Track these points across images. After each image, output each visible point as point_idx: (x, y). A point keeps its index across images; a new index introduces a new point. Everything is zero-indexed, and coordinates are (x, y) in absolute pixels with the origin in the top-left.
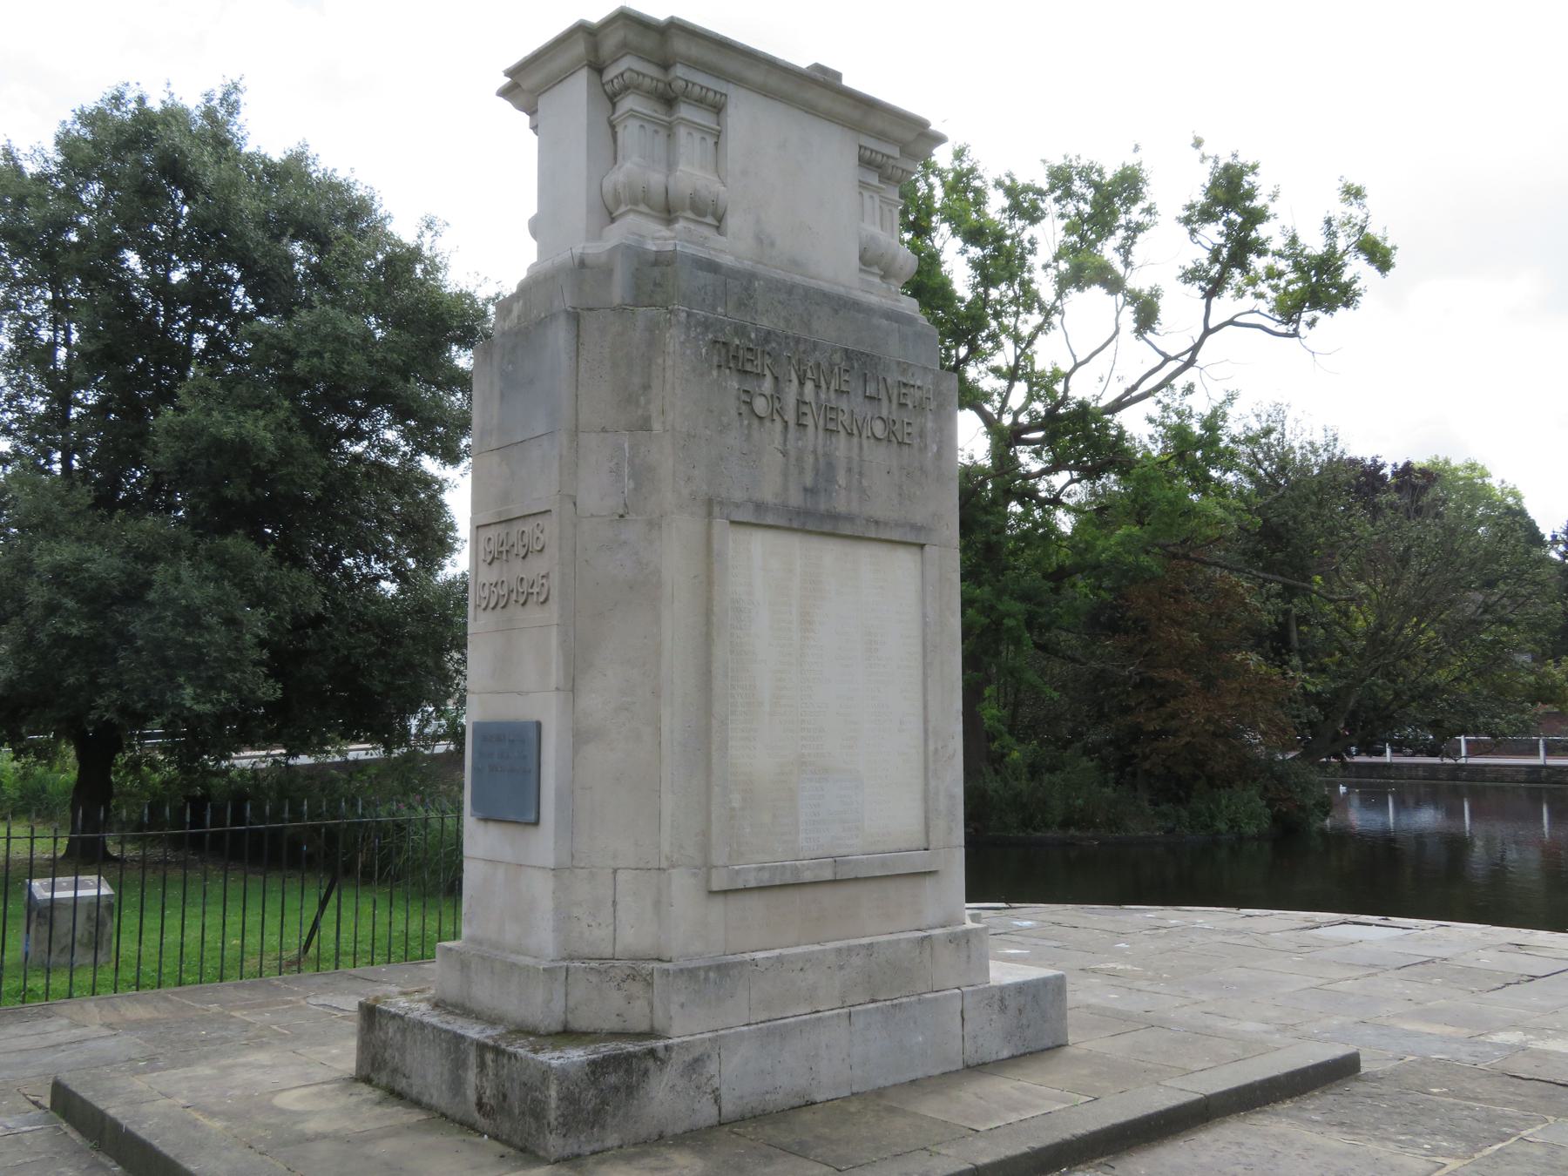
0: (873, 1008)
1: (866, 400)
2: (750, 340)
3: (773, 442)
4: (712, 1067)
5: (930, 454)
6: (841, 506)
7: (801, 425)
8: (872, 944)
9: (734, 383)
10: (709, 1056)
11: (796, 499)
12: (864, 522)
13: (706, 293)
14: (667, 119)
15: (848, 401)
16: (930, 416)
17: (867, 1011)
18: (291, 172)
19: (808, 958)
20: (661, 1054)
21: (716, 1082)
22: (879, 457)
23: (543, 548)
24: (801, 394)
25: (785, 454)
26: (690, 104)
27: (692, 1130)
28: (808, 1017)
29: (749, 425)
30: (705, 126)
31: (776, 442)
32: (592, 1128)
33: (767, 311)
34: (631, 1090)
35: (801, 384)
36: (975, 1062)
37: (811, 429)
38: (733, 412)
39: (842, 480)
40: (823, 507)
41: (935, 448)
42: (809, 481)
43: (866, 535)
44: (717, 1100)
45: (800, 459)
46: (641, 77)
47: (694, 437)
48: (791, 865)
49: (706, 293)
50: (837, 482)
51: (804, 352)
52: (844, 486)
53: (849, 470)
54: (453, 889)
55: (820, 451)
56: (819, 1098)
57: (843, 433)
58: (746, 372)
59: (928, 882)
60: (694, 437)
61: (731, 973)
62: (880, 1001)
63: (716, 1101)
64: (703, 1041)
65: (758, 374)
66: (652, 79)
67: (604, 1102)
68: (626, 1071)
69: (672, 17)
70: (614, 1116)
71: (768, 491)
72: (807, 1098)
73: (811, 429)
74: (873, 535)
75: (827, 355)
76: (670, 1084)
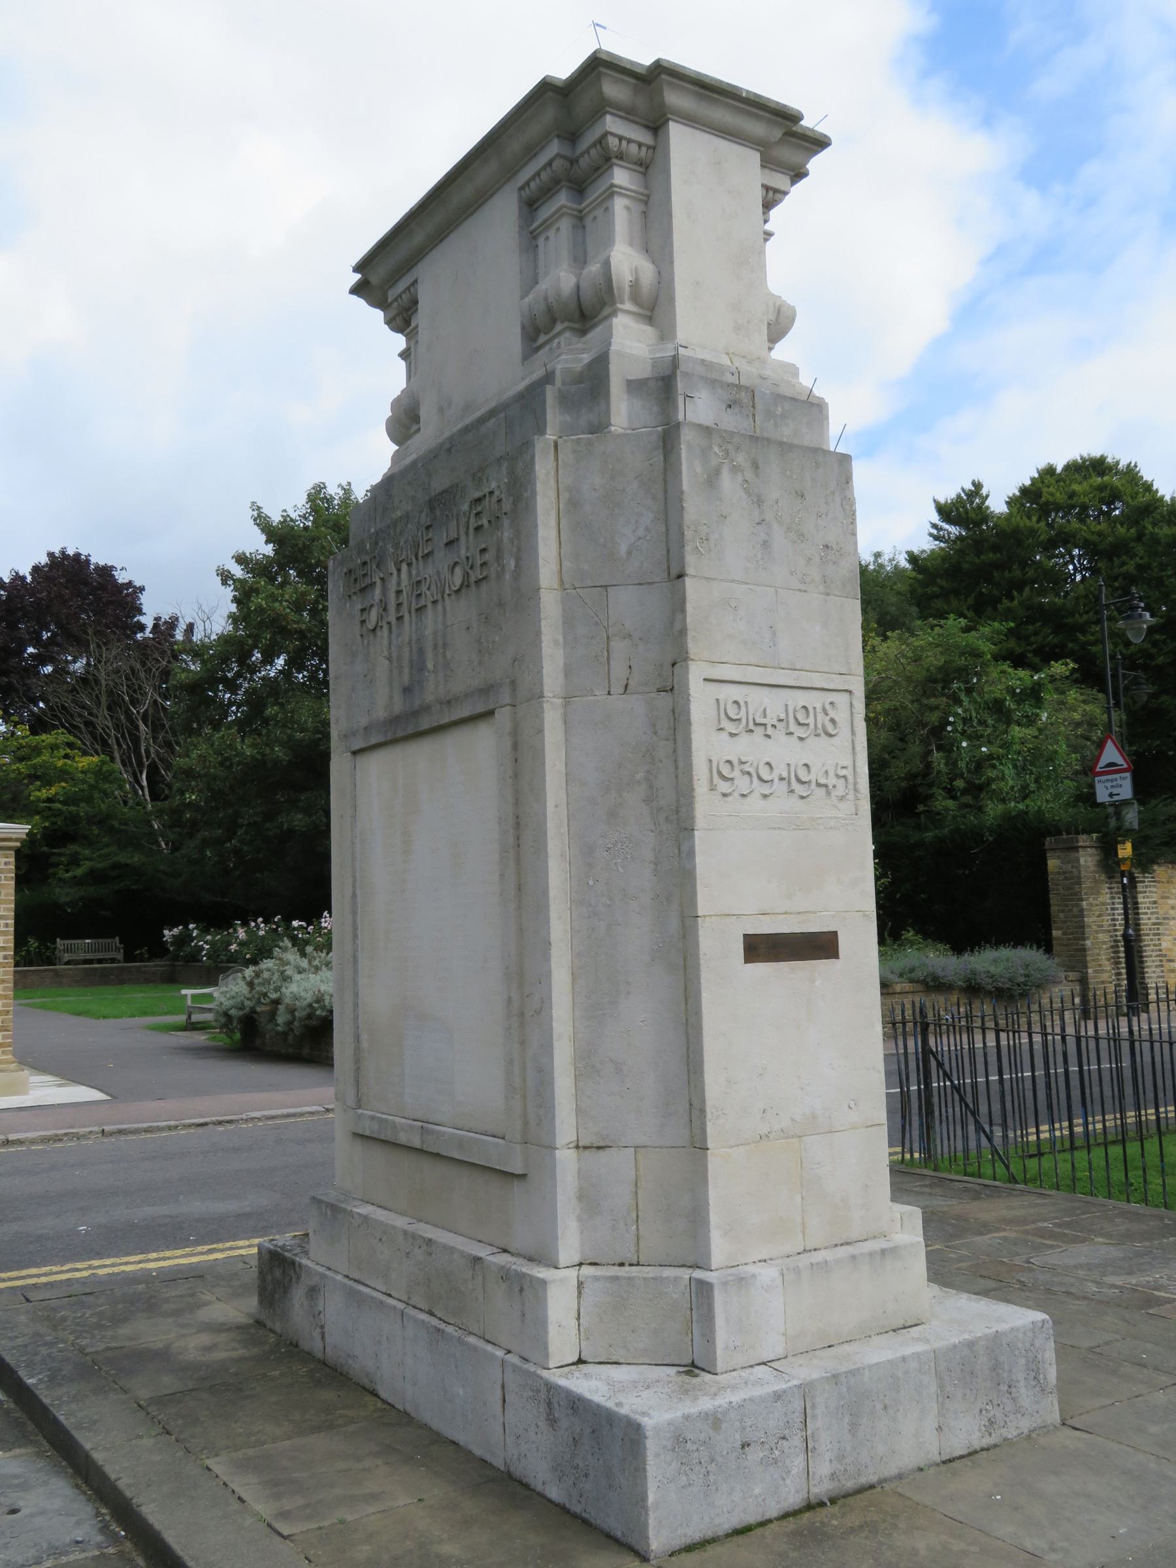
14: (576, 206)
23: (835, 735)
25: (390, 659)
39: (430, 666)
45: (399, 658)
54: (332, 1066)
56: (383, 1394)
59: (517, 1186)
66: (640, 145)
73: (407, 618)
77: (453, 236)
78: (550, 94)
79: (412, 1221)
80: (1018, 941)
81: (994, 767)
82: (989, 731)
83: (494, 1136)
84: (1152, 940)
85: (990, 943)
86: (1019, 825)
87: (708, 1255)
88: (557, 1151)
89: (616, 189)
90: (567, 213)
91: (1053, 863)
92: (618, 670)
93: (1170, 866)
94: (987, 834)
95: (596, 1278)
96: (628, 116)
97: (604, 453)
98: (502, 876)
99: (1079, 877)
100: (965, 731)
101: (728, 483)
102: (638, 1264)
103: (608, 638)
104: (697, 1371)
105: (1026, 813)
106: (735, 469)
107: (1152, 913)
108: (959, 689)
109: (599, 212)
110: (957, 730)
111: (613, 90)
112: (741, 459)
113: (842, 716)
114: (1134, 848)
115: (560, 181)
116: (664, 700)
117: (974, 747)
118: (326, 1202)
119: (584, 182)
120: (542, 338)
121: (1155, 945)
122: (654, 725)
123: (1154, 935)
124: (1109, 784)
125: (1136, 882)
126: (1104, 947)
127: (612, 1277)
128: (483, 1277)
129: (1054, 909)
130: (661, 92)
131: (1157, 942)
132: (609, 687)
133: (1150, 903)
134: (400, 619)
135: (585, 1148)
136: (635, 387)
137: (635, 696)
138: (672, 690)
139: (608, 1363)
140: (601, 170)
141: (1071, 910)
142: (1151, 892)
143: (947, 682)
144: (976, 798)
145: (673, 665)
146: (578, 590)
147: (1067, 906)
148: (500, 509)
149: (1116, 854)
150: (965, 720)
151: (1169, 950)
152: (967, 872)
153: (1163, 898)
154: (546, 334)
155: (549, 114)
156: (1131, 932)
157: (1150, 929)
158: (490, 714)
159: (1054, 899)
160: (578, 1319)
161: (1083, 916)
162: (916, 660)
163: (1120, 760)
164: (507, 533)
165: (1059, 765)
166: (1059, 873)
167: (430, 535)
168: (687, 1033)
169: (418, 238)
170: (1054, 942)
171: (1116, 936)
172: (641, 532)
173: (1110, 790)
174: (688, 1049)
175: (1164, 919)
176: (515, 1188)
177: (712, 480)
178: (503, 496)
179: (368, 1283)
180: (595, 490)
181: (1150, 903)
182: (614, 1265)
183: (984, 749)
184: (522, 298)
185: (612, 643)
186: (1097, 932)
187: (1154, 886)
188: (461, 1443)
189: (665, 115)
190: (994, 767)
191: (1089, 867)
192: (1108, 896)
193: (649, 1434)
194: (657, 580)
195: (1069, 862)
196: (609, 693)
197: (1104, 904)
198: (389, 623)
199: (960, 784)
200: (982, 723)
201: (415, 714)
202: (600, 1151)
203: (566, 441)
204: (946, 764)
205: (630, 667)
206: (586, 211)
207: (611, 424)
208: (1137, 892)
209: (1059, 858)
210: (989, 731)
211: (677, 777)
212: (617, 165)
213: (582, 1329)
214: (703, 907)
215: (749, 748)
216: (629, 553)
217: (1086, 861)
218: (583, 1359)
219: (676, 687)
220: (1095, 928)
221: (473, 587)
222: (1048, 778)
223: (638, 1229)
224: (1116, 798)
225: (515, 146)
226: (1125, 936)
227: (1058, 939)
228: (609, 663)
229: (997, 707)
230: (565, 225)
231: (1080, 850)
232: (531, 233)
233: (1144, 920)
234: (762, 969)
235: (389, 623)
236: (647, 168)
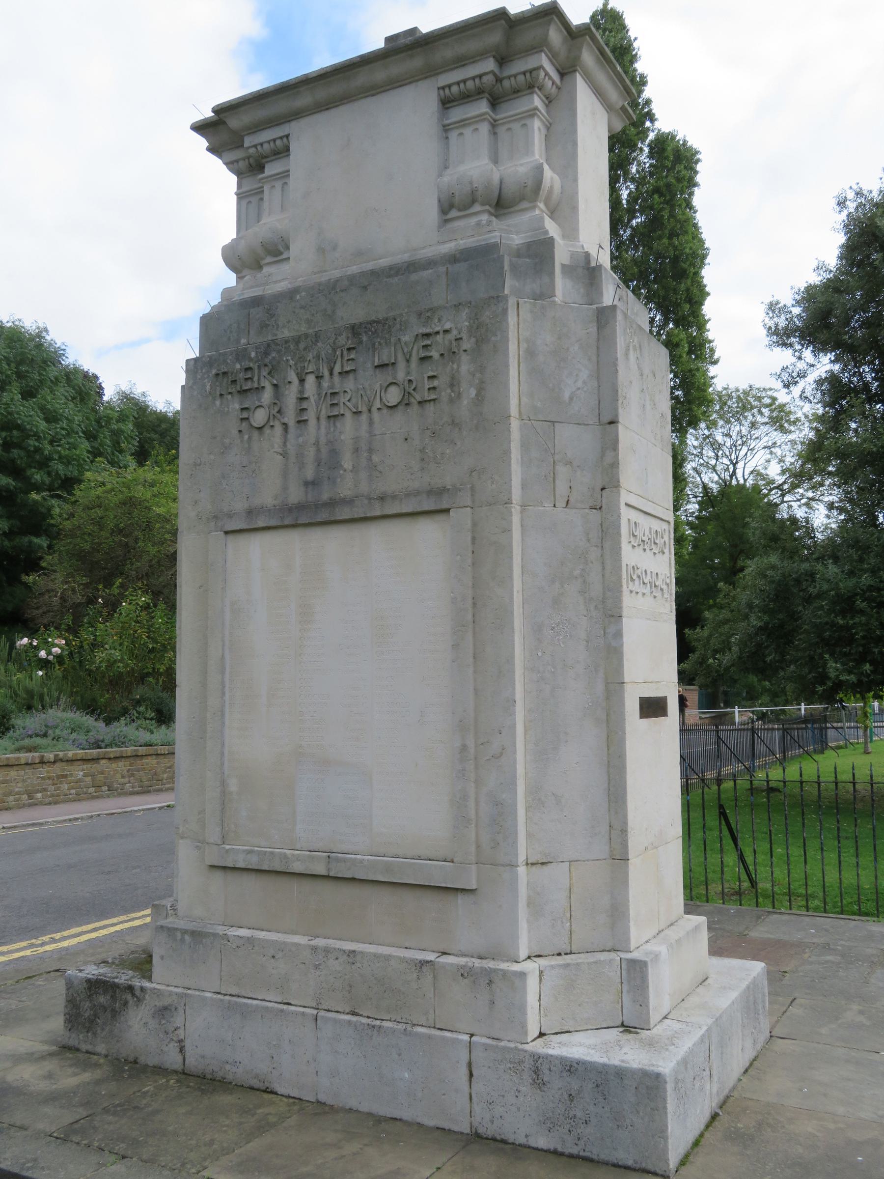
0: (344, 1020)
1: (378, 370)
2: (251, 360)
3: (273, 447)
4: (178, 1021)
5: (465, 402)
6: (345, 489)
8: (354, 951)
10: (176, 1009)
11: (296, 494)
12: (366, 502)
13: (231, 332)
15: (356, 379)
16: (465, 358)
17: (335, 1021)
19: (282, 947)
20: (138, 993)
21: (181, 1033)
24: (301, 392)
25: (284, 455)
26: (272, 161)
27: (160, 1068)
28: (276, 1005)
29: (250, 438)
30: (278, 174)
31: (276, 446)
32: (88, 1032)
33: (289, 322)
34: (115, 1014)
35: (302, 381)
36: (490, 1134)
37: (312, 422)
38: (235, 432)
40: (325, 496)
41: (473, 392)
42: (310, 473)
43: (368, 515)
44: (182, 1050)
45: (300, 456)
46: (235, 164)
47: (200, 465)
48: (280, 854)
49: (231, 332)
50: (341, 466)
51: (305, 349)
52: (351, 468)
53: (356, 450)
55: (323, 440)
56: (281, 1090)
57: (348, 415)
58: (246, 391)
60: (200, 465)
61: (204, 940)
62: (361, 1015)
63: (181, 1051)
64: (171, 994)
65: (257, 388)
67: (96, 1015)
68: (112, 997)
69: (504, 8)
70: (103, 1029)
71: (267, 497)
72: (267, 1084)
73: (312, 422)
74: (378, 513)
75: (331, 341)
76: (144, 1020)
77: (342, 109)
78: (503, 22)
79: (310, 938)
83: (430, 860)
87: (628, 940)
88: (518, 868)
89: (537, 112)
90: (488, 120)
92: (562, 487)
95: (553, 967)
96: (553, 59)
97: (554, 317)
98: (455, 646)
102: (571, 953)
103: (554, 462)
104: (639, 1031)
109: (516, 126)
111: (555, 36)
115: (483, 92)
116: (595, 515)
118: (181, 929)
119: (498, 98)
120: (454, 213)
122: (588, 534)
127: (564, 965)
128: (434, 977)
130: (580, 50)
132: (555, 501)
134: (301, 422)
135: (533, 864)
137: (574, 511)
138: (600, 508)
139: (562, 1033)
140: (519, 94)
145: (602, 489)
146: (533, 422)
148: (459, 346)
154: (460, 210)
155: (495, 38)
158: (447, 511)
160: (539, 1001)
164: (465, 366)
167: (352, 356)
168: (608, 772)
169: (304, 100)
172: (580, 384)
174: (609, 784)
176: (460, 902)
178: (464, 335)
179: (254, 996)
180: (547, 345)
182: (553, 955)
184: (440, 175)
185: (557, 467)
188: (405, 1118)
189: (575, 66)
193: (668, 1079)
194: (591, 423)
196: (554, 506)
198: (285, 425)
201: (318, 506)
202: (544, 866)
203: (525, 302)
205: (570, 487)
206: (500, 122)
207: (555, 296)
211: (603, 576)
212: (537, 93)
213: (542, 1009)
216: (571, 399)
218: (543, 1032)
219: (604, 507)
221: (416, 407)
223: (571, 925)
225: (447, 53)
228: (554, 482)
232: (444, 126)
235: (285, 425)
236: (550, 102)
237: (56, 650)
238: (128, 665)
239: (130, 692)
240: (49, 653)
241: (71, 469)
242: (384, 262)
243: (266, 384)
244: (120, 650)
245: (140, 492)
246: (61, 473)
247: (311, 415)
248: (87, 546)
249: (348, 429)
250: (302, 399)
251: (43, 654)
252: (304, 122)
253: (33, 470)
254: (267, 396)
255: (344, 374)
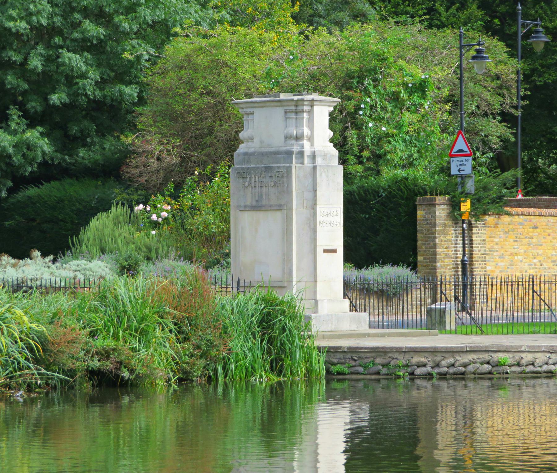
7: (255, 187)
9: (242, 181)
11: (254, 203)
18: (331, 127)
22: (272, 190)
25: (252, 194)
39: (264, 197)
40: (260, 204)
42: (257, 198)
45: (255, 194)
71: (248, 203)
80: (395, 263)
81: (390, 142)
82: (388, 115)
84: (480, 264)
85: (379, 263)
86: (402, 187)
91: (420, 214)
93: (497, 216)
94: (382, 191)
99: (435, 223)
100: (371, 115)
101: (323, 174)
105: (407, 179)
106: (325, 172)
107: (481, 247)
108: (369, 84)
110: (366, 114)
112: (325, 170)
113: (339, 212)
114: (472, 204)
116: (312, 211)
117: (376, 127)
121: (482, 268)
123: (482, 261)
124: (459, 163)
125: (472, 227)
126: (448, 267)
129: (419, 243)
131: (484, 266)
133: (481, 240)
136: (308, 156)
141: (429, 244)
142: (482, 233)
143: (361, 78)
144: (376, 163)
147: (427, 241)
149: (460, 209)
150: (372, 107)
151: (492, 271)
152: (367, 216)
153: (490, 237)
156: (466, 258)
157: (480, 258)
159: (420, 237)
161: (436, 248)
162: (340, 58)
163: (466, 149)
165: (435, 142)
166: (423, 220)
170: (418, 264)
171: (457, 261)
173: (459, 167)
175: (490, 251)
177: (321, 174)
181: (481, 240)
183: (384, 129)
186: (444, 258)
187: (485, 230)
190: (390, 142)
191: (442, 217)
192: (453, 235)
195: (430, 213)
197: (450, 240)
199: (366, 154)
200: (384, 109)
204: (358, 139)
208: (472, 234)
209: (424, 210)
210: (388, 115)
214: (318, 245)
215: (325, 219)
217: (440, 213)
220: (443, 255)
222: (427, 151)
224: (462, 173)
226: (463, 261)
227: (421, 262)
229: (395, 98)
230: (294, 120)
231: (437, 206)
233: (476, 251)
234: (326, 254)
237: (164, 214)
238: (219, 226)
239: (221, 248)
240: (159, 216)
241: (158, 14)
242: (273, 149)
243: (248, 177)
244: (213, 215)
245: (227, 55)
246: (149, 19)
247: (257, 186)
248: (178, 108)
249: (264, 190)
250: (255, 182)
251: (154, 217)
252: (257, 109)
253: (121, 17)
254: (248, 179)
255: (263, 177)
